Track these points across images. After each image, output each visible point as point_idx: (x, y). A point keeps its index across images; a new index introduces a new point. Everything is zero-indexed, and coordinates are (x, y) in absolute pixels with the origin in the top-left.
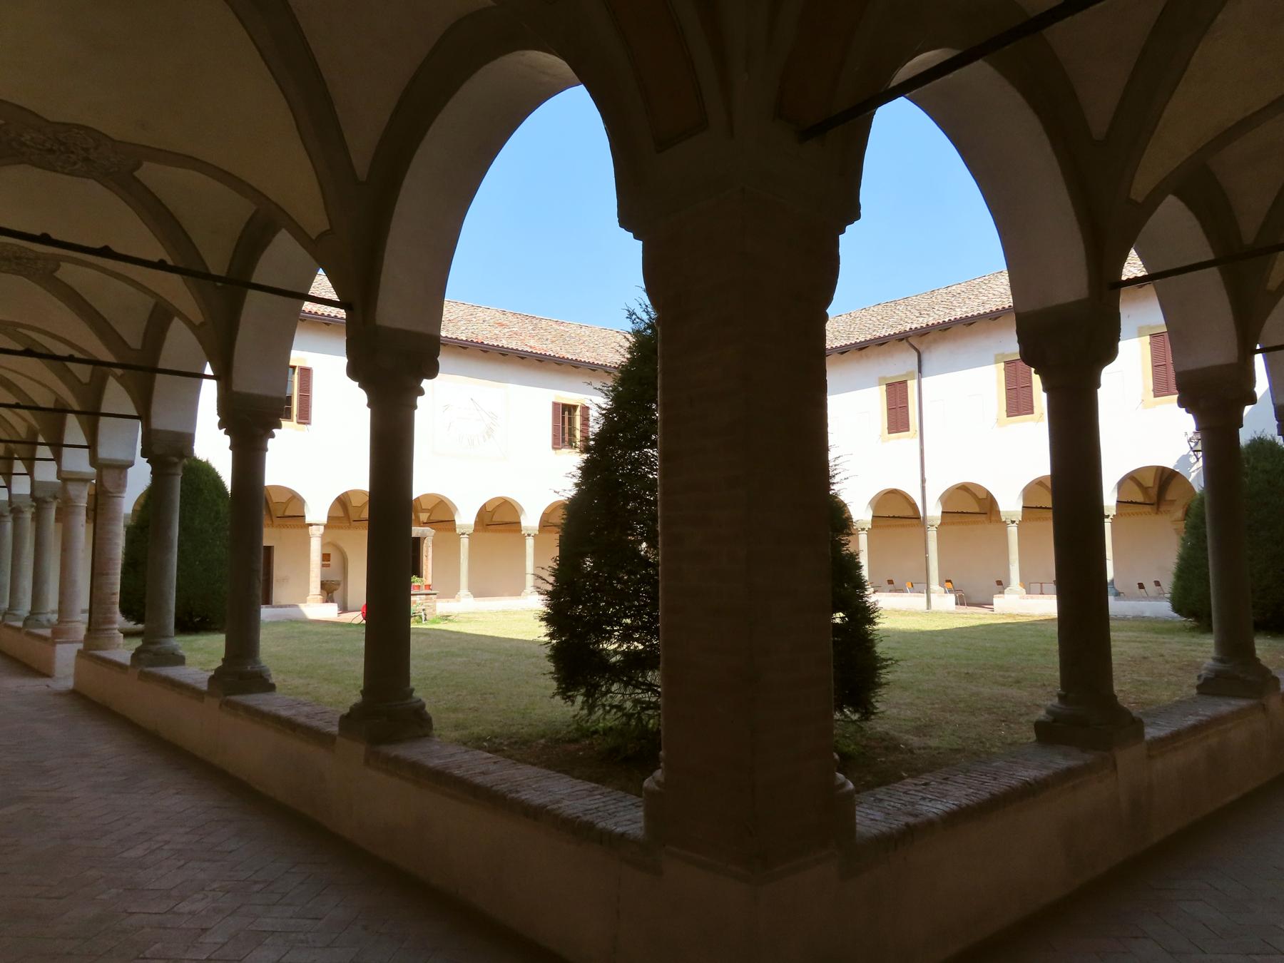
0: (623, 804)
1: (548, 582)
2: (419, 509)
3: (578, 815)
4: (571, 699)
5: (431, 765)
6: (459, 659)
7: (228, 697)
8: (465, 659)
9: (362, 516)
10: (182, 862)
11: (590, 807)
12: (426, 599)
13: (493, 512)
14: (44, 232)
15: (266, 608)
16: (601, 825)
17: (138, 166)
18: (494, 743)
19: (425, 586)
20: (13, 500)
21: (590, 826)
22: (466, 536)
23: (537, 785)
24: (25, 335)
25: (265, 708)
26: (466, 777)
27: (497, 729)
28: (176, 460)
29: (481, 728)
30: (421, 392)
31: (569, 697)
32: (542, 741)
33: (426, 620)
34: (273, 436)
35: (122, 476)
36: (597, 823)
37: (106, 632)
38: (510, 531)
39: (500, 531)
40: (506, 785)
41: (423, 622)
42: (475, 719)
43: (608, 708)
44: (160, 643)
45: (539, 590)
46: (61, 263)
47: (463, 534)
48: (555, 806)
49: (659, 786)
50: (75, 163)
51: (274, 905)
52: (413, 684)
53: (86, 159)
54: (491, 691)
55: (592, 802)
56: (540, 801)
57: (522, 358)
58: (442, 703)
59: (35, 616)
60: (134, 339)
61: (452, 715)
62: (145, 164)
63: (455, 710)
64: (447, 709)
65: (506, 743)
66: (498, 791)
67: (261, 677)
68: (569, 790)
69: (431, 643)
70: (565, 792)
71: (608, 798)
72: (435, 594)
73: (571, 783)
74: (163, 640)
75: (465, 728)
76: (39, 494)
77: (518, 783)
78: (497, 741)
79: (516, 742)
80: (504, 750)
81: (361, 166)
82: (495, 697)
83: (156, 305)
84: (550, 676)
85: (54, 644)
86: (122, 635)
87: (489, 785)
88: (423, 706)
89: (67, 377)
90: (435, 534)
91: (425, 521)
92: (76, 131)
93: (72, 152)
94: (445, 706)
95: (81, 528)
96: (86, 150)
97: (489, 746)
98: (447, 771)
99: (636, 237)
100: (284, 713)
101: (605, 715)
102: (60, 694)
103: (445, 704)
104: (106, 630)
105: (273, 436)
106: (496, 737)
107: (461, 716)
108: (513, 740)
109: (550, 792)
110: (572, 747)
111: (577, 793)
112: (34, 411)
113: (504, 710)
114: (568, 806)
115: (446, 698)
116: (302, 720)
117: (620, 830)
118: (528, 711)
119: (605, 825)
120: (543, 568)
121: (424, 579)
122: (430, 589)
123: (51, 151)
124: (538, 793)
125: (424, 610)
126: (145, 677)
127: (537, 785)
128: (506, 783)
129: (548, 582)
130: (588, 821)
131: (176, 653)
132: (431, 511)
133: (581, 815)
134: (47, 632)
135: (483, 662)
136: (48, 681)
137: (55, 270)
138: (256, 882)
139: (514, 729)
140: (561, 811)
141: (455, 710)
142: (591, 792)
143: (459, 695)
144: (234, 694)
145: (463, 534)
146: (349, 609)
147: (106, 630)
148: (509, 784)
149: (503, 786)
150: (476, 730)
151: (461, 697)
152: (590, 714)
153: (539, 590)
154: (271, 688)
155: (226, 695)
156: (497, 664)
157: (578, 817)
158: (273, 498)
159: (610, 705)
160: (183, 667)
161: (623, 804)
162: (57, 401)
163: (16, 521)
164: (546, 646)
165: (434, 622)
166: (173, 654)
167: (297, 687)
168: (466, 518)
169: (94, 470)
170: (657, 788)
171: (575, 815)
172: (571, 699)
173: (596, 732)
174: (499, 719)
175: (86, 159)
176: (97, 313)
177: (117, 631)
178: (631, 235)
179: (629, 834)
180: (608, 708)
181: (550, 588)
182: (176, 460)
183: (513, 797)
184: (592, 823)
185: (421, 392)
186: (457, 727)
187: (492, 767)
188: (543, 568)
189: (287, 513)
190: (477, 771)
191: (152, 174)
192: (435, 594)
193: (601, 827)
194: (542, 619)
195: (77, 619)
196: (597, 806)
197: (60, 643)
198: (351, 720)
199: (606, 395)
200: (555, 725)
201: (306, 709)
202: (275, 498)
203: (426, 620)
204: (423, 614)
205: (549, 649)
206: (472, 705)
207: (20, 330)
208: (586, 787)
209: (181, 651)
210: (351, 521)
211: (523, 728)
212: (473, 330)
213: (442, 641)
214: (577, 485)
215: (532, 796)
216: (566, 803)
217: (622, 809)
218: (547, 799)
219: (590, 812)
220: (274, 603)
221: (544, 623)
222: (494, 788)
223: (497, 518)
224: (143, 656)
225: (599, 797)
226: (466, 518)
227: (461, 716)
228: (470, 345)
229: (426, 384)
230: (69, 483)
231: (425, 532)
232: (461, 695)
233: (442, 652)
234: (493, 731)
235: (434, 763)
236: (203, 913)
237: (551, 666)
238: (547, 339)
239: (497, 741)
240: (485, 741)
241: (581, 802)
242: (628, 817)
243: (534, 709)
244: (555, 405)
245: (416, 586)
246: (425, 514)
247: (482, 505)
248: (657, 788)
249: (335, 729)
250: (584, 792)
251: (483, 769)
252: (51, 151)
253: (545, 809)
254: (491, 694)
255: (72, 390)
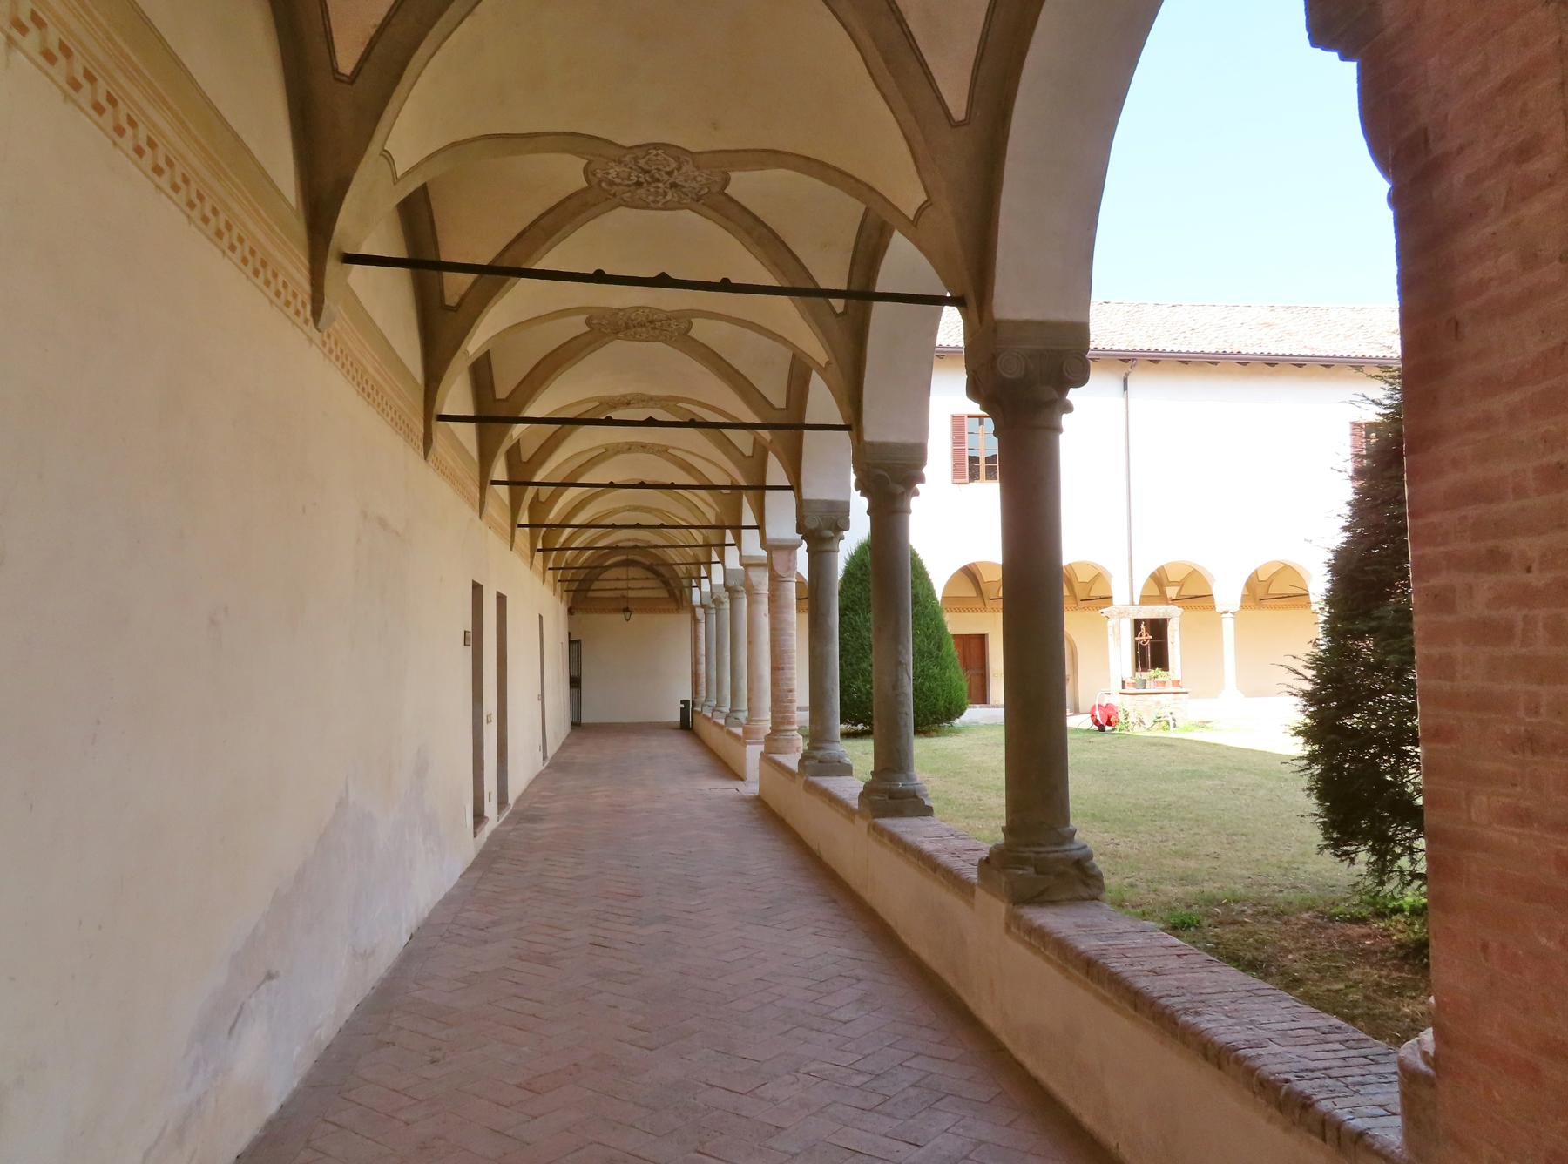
0: (1379, 1069)
1: (1306, 678)
2: (1165, 581)
3: (1286, 1076)
4: (1350, 857)
5: (1082, 947)
6: (1210, 783)
7: (876, 820)
8: (1217, 782)
9: (1091, 595)
10: (789, 1027)
11: (1313, 1065)
12: (1175, 700)
13: (1269, 582)
14: (599, 268)
15: (981, 707)
16: (1325, 1106)
17: (727, 181)
18: (1232, 910)
19: (1173, 682)
20: (714, 591)
21: (1305, 1103)
22: (1229, 615)
23: (1233, 1006)
24: (686, 409)
25: (909, 838)
26: (1124, 975)
27: (1240, 889)
28: (831, 534)
29: (1217, 885)
30: (1068, 408)
31: (1347, 853)
32: (1306, 916)
33: (1175, 726)
34: (917, 493)
35: (792, 557)
36: (1318, 1101)
37: (784, 734)
38: (1295, 606)
39: (1279, 607)
40: (1183, 999)
41: (1172, 729)
42: (1212, 870)
43: (1409, 878)
44: (823, 748)
45: (1289, 689)
46: (693, 320)
47: (1225, 612)
48: (1250, 1052)
49: (1427, 1063)
50: (665, 194)
51: (870, 1110)
52: (1074, 823)
53: (674, 186)
54: (1245, 831)
55: (1320, 1055)
56: (1229, 1038)
57: (1300, 366)
58: (1170, 843)
59: (734, 714)
60: (779, 400)
61: (1180, 862)
62: (734, 175)
63: (1187, 856)
64: (1176, 852)
65: (1250, 912)
66: (1167, 1006)
67: (916, 797)
68: (1286, 1026)
69: (1174, 758)
70: (1279, 1026)
71: (1353, 1053)
72: (1186, 693)
73: (1294, 1011)
74: (827, 745)
75: (1194, 883)
76: (731, 583)
77: (1203, 998)
78: (1237, 907)
79: (1266, 913)
80: (1246, 922)
81: (957, 105)
82: (1248, 841)
83: (794, 356)
84: (1311, 819)
85: (745, 744)
86: (801, 737)
87: (1155, 995)
88: (1089, 856)
89: (728, 447)
90: (1182, 614)
91: (1174, 598)
92: (655, 152)
93: (658, 180)
94: (1173, 848)
95: (764, 617)
96: (670, 173)
97: (1223, 914)
98: (1102, 961)
99: (1343, 58)
100: (928, 847)
101: (1403, 888)
102: (745, 800)
103: (1175, 845)
104: (787, 731)
105: (917, 493)
106: (1236, 902)
107: (1192, 864)
108: (1261, 909)
109: (1252, 1022)
110: (1356, 930)
111: (1300, 1032)
112: (712, 491)
113: (1258, 860)
114: (1275, 1055)
115: (1177, 836)
116: (944, 858)
117: (1358, 1123)
118: (1295, 866)
119: (1331, 1106)
120: (1295, 657)
121: (1170, 672)
122: (1179, 686)
123: (639, 184)
124: (1231, 1021)
125: (1171, 713)
126: (812, 788)
127: (1233, 1006)
128: (1184, 995)
129: (1306, 678)
130: (1302, 1092)
131: (842, 760)
132: (1181, 584)
133: (1291, 1077)
134: (739, 731)
135: (1241, 788)
136: (739, 784)
137: (689, 329)
138: (859, 1072)
139: (1266, 892)
140: (1258, 1063)
141: (1187, 856)
142: (1324, 1035)
143: (1196, 834)
144: (884, 816)
145: (1225, 612)
146: (1081, 710)
147: (787, 731)
148: (1188, 997)
149: (1176, 999)
150: (1210, 888)
151: (1197, 837)
152: (1382, 883)
153: (1289, 689)
154: (928, 811)
155: (874, 817)
156: (1262, 792)
157: (1287, 1081)
158: (984, 576)
159: (1411, 874)
160: (849, 778)
161: (1379, 1069)
162: (732, 482)
163: (718, 611)
164: (1302, 773)
165: (1186, 730)
166: (839, 762)
167: (991, 809)
168: (1228, 593)
169: (764, 553)
170: (1422, 1066)
171: (1283, 1076)
172: (1350, 857)
173: (1399, 910)
174: (1246, 874)
175: (674, 186)
176: (737, 372)
177: (796, 733)
178: (1334, 55)
179: (1374, 1137)
180: (1409, 878)
181: (1308, 687)
182: (831, 534)
183: (1187, 1021)
184: (1309, 1098)
185: (1068, 408)
186: (1183, 880)
187: (1173, 963)
188: (1295, 657)
189: (1093, 594)
190: (1145, 968)
191: (745, 185)
192: (1186, 693)
193: (1324, 1109)
194: (1299, 733)
195: (764, 719)
196: (1327, 1064)
197: (750, 743)
198: (994, 863)
199: (1391, 384)
200: (1333, 892)
201: (958, 843)
202: (1083, 576)
203: (1175, 726)
204: (1170, 719)
205: (1307, 778)
206: (1212, 850)
207: (680, 404)
208: (1317, 1023)
209: (848, 759)
210: (1079, 601)
211: (1281, 891)
212: (1226, 338)
213: (1191, 755)
214: (1345, 529)
215: (1218, 1026)
216: (1276, 1048)
217: (1374, 1079)
218: (1242, 1036)
219: (1311, 1075)
220: (992, 702)
221: (1301, 740)
222: (1163, 1001)
223: (1274, 590)
224: (807, 763)
225: (1337, 1046)
226: (1228, 593)
227: (1192, 864)
228: (1222, 359)
229: (1073, 395)
230: (750, 569)
231: (1169, 610)
232: (1199, 834)
233: (1188, 771)
234: (1234, 892)
235: (1087, 944)
236: (787, 1104)
237: (1312, 804)
238: (1338, 335)
239: (1237, 907)
240: (1219, 905)
241: (1299, 1050)
242: (1380, 1099)
243: (1304, 863)
244: (1355, 425)
245: (1161, 682)
246: (1173, 588)
247: (1253, 570)
248: (1422, 1066)
249: (973, 876)
250: (1312, 1032)
251: (1157, 964)
252: (639, 184)
253: (1234, 1054)
254: (1243, 834)
255: (736, 463)
